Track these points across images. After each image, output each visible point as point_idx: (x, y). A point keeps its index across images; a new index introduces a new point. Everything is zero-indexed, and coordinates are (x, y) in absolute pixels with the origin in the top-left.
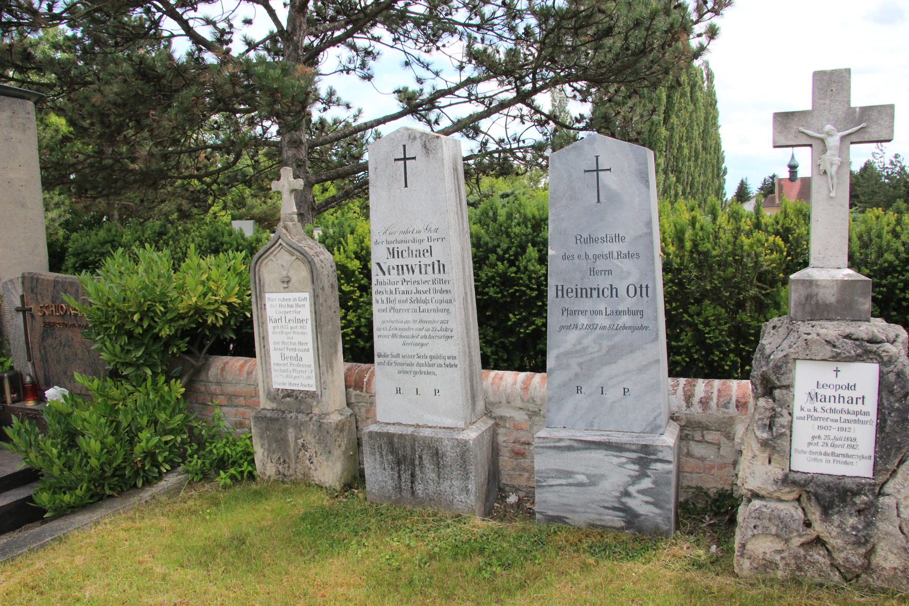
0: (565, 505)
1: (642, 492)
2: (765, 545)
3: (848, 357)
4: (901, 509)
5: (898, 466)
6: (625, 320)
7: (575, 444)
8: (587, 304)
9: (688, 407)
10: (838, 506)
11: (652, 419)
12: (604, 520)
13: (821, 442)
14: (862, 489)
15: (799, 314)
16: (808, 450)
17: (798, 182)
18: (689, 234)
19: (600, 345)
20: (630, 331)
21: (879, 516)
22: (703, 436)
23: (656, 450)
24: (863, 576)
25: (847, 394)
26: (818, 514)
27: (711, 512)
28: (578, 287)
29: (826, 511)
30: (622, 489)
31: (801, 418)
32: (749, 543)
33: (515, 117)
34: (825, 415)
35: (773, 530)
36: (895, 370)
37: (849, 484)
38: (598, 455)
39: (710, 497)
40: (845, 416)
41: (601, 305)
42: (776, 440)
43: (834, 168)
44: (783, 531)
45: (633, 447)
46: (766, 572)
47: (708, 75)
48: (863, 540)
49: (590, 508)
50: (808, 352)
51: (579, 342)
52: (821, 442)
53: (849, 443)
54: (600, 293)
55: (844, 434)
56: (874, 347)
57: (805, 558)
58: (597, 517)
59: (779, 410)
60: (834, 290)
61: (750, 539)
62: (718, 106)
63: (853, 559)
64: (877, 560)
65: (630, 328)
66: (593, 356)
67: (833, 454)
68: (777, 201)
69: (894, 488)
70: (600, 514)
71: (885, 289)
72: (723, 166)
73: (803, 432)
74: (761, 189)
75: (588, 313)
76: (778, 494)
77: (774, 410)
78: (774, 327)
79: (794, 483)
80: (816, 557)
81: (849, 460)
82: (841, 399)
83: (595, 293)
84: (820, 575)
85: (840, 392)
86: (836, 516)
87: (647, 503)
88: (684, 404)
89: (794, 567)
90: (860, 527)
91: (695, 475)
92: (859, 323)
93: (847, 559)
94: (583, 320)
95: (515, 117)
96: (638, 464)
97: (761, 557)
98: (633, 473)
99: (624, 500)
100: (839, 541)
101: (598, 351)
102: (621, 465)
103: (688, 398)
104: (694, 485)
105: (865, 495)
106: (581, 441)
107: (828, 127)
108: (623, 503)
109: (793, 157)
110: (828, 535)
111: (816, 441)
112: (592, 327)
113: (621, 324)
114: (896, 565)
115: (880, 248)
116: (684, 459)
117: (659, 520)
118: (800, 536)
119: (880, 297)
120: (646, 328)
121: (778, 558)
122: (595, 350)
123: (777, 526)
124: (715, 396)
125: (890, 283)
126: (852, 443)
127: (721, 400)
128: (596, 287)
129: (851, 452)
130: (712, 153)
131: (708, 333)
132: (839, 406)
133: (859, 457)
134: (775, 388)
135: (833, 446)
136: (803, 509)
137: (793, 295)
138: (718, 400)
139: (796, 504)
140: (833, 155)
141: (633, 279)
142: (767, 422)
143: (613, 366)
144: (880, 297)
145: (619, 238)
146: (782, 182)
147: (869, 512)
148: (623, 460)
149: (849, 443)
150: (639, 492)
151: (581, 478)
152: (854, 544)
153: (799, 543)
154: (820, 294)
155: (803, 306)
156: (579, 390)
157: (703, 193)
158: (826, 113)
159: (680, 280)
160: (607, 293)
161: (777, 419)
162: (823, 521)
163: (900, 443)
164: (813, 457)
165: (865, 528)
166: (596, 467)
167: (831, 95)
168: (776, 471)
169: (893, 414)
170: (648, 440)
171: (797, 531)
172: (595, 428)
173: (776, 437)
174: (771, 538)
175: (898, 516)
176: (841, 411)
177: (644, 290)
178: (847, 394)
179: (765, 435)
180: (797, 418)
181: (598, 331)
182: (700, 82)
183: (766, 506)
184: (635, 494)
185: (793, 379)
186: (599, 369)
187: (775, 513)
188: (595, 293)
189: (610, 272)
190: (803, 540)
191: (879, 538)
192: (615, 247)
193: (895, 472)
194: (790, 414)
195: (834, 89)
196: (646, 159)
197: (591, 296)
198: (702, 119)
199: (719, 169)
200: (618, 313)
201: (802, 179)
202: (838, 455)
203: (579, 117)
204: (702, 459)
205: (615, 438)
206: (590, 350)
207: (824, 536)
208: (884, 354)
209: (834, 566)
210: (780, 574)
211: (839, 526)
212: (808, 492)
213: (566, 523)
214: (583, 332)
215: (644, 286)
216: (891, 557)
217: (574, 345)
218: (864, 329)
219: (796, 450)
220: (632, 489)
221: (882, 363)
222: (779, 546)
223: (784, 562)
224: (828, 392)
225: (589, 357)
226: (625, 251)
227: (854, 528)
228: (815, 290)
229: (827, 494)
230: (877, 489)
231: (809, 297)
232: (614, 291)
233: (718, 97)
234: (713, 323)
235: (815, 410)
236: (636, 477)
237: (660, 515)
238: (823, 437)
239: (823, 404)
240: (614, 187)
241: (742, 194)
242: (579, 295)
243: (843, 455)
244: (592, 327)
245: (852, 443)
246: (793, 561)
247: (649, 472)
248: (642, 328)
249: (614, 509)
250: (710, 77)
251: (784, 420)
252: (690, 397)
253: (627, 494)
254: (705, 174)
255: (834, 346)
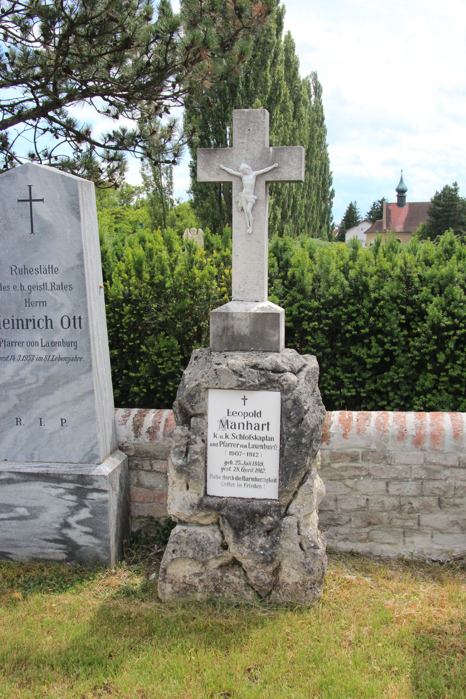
0: (7, 540)
1: (80, 522)
2: (185, 569)
3: (252, 385)
4: (302, 528)
5: (299, 487)
6: (61, 351)
7: (15, 477)
8: (23, 335)
9: (136, 437)
10: (248, 528)
11: (89, 449)
12: (46, 553)
13: (232, 467)
14: (267, 511)
15: (217, 346)
16: (222, 475)
17: (406, 208)
18: (145, 267)
19: (37, 376)
20: (65, 362)
21: (283, 534)
22: (151, 465)
23: (92, 480)
24: (273, 592)
25: (253, 420)
26: (231, 536)
27: (143, 538)
28: (15, 318)
29: (238, 531)
30: (61, 520)
31: (214, 445)
32: (170, 567)
33: (45, 131)
34: (236, 441)
35: (191, 554)
36: (292, 398)
37: (257, 506)
38: (37, 487)
39: (160, 526)
40: (253, 442)
41: (37, 337)
42: (193, 465)
43: (250, 206)
44: (200, 553)
45: (70, 478)
46: (187, 595)
47: (315, 88)
48: (269, 559)
49: (32, 541)
50: (217, 381)
51: (17, 373)
52: (232, 467)
53: (257, 467)
54: (36, 324)
55: (253, 459)
56: (276, 376)
57: (222, 579)
58: (39, 550)
59: (193, 437)
60: (248, 323)
61: (170, 563)
62: (326, 123)
63: (263, 577)
64: (283, 576)
65: (65, 359)
66: (30, 387)
67: (244, 478)
68: (385, 227)
69: (296, 508)
70: (41, 547)
71: (330, 321)
72: (330, 189)
73: (217, 457)
74: (370, 213)
75: (25, 345)
76: (194, 519)
77: (189, 437)
78: (196, 358)
79: (208, 507)
80: (232, 577)
81: (258, 483)
82: (249, 425)
83: (31, 325)
84: (236, 595)
85: (248, 419)
86: (246, 537)
87: (86, 533)
88: (133, 434)
89: (212, 589)
90: (267, 546)
91: (146, 505)
92: (268, 354)
93: (257, 578)
94: (20, 351)
95: (45, 131)
96: (75, 494)
97: (181, 581)
98: (71, 504)
99: (65, 531)
100: (250, 561)
101: (35, 383)
102: (59, 496)
103: (137, 428)
104: (146, 515)
105: (271, 515)
106: (20, 473)
107: (244, 166)
108: (63, 535)
109: (401, 181)
110: (240, 555)
111: (228, 466)
112: (29, 358)
113: (56, 355)
114: (297, 580)
115: (328, 281)
116: (134, 489)
117: (99, 550)
118: (217, 558)
119: (327, 328)
120: (81, 359)
121: (196, 580)
122: (33, 381)
123: (194, 549)
124: (162, 426)
125: (336, 315)
126: (260, 467)
127: (168, 429)
128: (32, 318)
129: (259, 475)
130: (318, 174)
131: (162, 364)
132: (247, 433)
133: (266, 480)
134: (191, 417)
135: (243, 470)
136: (222, 532)
137: (214, 326)
138: (165, 429)
139: (217, 527)
140: (248, 193)
141: (66, 311)
142: (184, 449)
143: (51, 397)
144: (327, 328)
145: (52, 270)
146: (390, 207)
147: (273, 531)
148: (61, 491)
149: (257, 467)
150: (78, 522)
151: (22, 511)
152: (262, 563)
153: (216, 566)
154: (236, 326)
155: (221, 337)
156: (18, 421)
157: (306, 217)
158: (244, 151)
159: (138, 311)
160: (42, 324)
161: (191, 446)
162: (236, 542)
163: (297, 466)
164: (226, 481)
165: (271, 547)
166: (35, 499)
167: (248, 135)
168: (193, 496)
169: (290, 439)
170: (84, 470)
171: (214, 553)
172: (35, 460)
173: (190, 463)
174: (189, 562)
175: (299, 534)
176: (249, 438)
177: (77, 321)
178: (253, 420)
179: (180, 462)
180: (211, 445)
181: (35, 363)
182: (307, 97)
183: (184, 531)
184: (74, 525)
185: (206, 407)
186: (37, 400)
187: (193, 537)
188: (31, 325)
189: (44, 303)
190: (220, 562)
191: (283, 556)
192: (49, 279)
193: (296, 493)
194: (203, 441)
195: (251, 129)
196: (77, 191)
197: (27, 328)
198: (307, 137)
199: (326, 191)
200: (54, 344)
201: (412, 205)
202: (248, 479)
203: (112, 134)
204: (151, 488)
205: (54, 469)
206: (28, 381)
207: (237, 556)
208: (284, 383)
209: (249, 585)
210: (199, 596)
211: (249, 547)
212: (222, 516)
213: (8, 558)
214: (21, 363)
215: (77, 317)
216: (293, 572)
217: (12, 377)
218: (268, 360)
219: (211, 475)
220: (71, 520)
221: (284, 392)
222: (197, 569)
223: (202, 584)
224: (238, 419)
225: (25, 389)
226: (58, 283)
227: (262, 548)
228: (231, 322)
229: (238, 516)
230: (283, 510)
231: (226, 329)
232: (49, 322)
233: (326, 113)
234: (164, 354)
235: (227, 437)
236: (75, 507)
237: (99, 545)
238: (234, 462)
239: (233, 431)
240: (47, 217)
241: (351, 219)
242: (16, 326)
243: (253, 479)
244: (29, 358)
245: (260, 467)
246: (211, 583)
247: (87, 502)
248: (76, 359)
249: (55, 541)
250: (318, 90)
251: (197, 447)
252: (138, 427)
253: (66, 525)
254: (309, 197)
255: (241, 376)
